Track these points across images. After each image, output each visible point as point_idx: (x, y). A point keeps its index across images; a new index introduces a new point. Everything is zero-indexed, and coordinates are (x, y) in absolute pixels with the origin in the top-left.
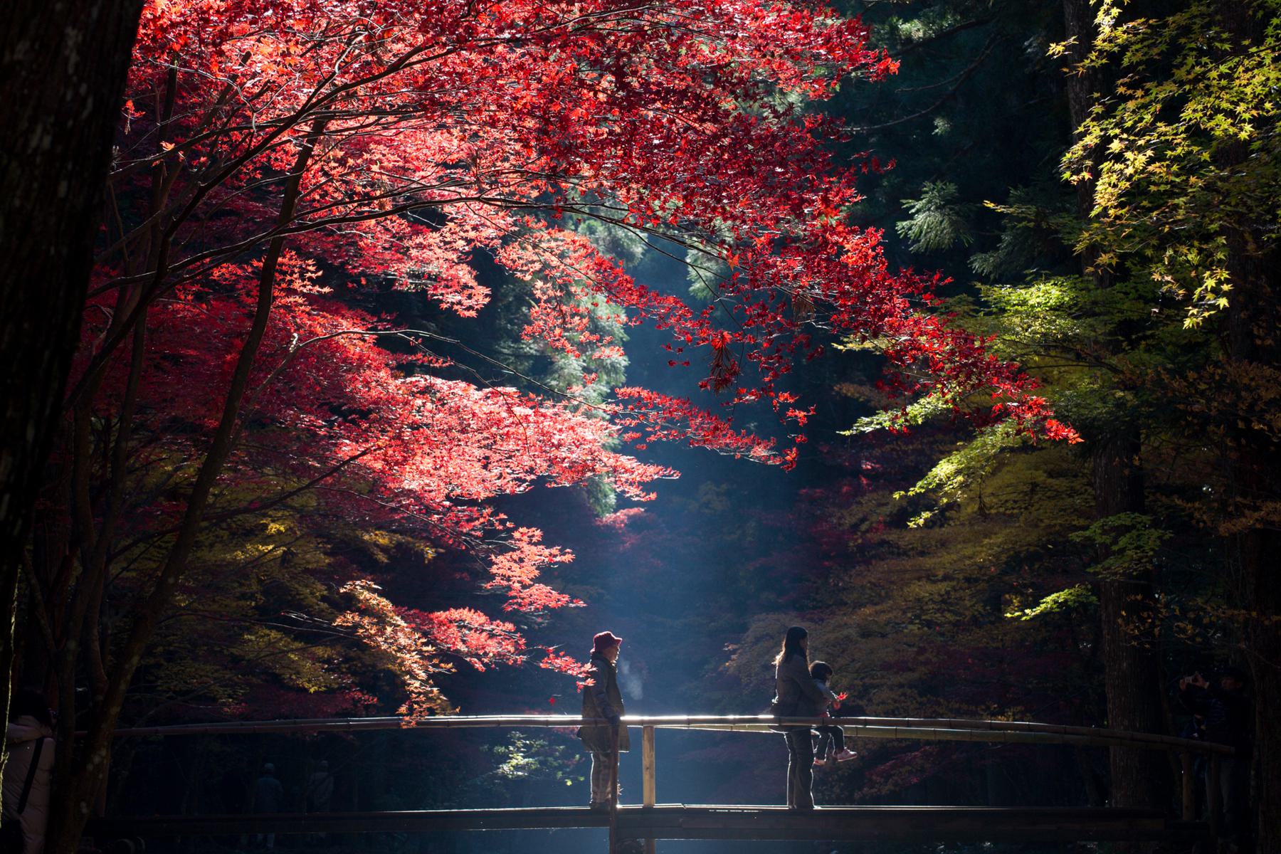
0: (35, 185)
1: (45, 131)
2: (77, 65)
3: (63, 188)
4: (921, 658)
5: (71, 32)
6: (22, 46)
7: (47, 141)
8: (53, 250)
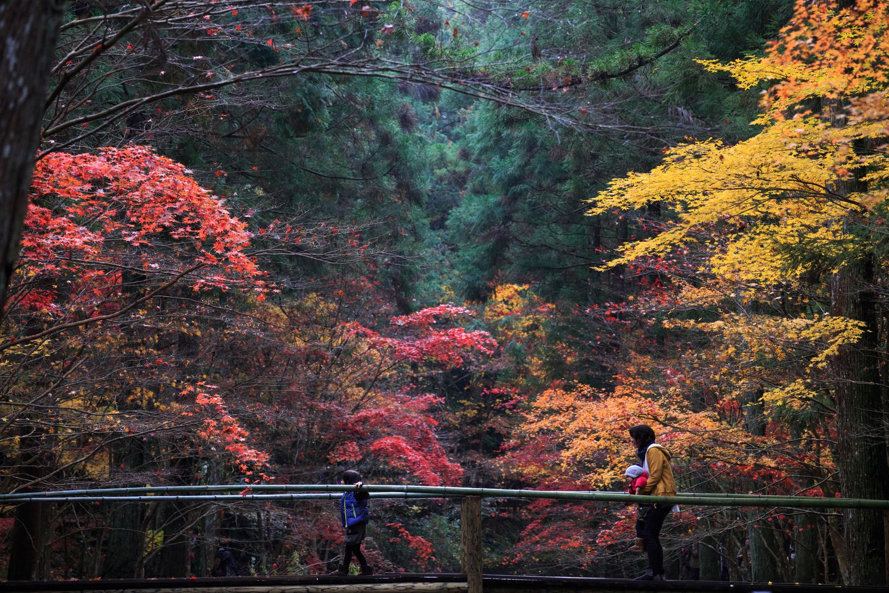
2: (16, 66)
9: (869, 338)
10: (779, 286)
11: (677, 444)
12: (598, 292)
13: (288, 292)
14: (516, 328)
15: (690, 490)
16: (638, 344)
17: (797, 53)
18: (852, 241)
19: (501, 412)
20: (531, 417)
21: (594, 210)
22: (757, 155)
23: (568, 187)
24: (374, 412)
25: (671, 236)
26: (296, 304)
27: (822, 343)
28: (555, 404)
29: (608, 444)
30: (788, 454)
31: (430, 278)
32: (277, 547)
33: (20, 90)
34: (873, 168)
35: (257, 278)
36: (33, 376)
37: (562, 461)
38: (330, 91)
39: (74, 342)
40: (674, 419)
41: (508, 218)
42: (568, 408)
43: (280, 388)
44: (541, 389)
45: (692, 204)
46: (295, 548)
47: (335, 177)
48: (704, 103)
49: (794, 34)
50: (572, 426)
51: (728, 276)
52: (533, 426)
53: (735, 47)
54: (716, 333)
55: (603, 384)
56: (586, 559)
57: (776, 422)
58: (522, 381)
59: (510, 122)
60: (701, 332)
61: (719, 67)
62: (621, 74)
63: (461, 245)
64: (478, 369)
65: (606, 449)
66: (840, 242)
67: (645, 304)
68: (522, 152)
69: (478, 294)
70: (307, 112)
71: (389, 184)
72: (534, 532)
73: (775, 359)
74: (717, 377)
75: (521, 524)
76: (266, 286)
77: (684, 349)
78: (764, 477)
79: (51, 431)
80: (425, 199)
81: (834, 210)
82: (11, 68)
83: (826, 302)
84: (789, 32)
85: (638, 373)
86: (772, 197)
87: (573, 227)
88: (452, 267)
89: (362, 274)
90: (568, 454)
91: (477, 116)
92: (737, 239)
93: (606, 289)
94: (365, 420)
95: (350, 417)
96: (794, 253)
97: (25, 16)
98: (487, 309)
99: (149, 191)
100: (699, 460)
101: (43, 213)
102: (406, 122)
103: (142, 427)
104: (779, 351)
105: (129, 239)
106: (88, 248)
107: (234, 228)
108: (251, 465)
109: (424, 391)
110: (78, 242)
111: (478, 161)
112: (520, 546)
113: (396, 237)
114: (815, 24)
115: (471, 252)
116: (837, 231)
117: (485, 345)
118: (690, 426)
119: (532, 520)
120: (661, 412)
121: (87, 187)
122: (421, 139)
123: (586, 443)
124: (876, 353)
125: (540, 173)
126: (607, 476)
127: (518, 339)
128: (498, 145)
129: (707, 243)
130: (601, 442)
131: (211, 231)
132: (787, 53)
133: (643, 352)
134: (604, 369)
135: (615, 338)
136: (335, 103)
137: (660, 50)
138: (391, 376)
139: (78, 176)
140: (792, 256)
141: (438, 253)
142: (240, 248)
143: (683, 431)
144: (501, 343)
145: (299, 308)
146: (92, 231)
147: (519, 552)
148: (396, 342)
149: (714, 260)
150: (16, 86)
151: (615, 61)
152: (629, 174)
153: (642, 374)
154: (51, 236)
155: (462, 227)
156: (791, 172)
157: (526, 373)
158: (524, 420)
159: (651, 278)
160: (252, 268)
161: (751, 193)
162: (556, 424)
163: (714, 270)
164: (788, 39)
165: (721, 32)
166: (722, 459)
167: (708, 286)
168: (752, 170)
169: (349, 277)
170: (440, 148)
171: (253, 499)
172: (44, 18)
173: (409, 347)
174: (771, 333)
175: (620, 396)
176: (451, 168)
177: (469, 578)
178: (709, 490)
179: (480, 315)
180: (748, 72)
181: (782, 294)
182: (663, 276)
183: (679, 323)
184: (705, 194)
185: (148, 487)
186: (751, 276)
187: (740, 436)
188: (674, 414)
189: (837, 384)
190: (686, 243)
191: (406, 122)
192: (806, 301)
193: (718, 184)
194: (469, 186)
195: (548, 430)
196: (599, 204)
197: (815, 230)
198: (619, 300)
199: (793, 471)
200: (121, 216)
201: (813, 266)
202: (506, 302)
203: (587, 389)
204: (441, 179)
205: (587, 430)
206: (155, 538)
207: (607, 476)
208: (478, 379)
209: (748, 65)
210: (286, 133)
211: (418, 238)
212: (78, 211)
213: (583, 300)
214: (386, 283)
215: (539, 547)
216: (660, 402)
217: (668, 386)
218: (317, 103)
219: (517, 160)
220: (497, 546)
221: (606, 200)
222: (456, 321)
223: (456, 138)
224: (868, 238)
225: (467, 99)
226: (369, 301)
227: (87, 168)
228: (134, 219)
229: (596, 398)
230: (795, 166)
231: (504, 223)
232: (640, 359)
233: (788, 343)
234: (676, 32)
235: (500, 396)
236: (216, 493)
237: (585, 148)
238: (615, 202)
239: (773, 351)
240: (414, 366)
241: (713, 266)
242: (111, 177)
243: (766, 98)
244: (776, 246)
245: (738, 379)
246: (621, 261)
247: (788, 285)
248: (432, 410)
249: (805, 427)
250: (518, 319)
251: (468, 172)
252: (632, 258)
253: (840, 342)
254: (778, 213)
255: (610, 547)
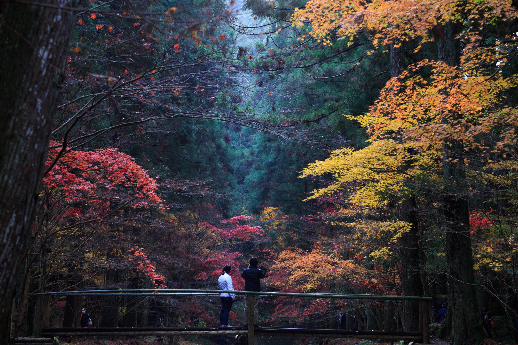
0: (28, 145)
1: (31, 130)
2: (41, 110)
3: (36, 146)
4: (463, 7)
5: (39, 100)
6: (25, 105)
7: (32, 133)
8: (33, 165)
9: (414, 230)
10: (378, 208)
11: (337, 273)
12: (306, 211)
13: (179, 210)
14: (273, 225)
15: (343, 292)
16: (322, 232)
17: (382, 111)
18: (407, 190)
19: (266, 260)
20: (277, 262)
21: (302, 176)
22: (369, 154)
23: (294, 167)
24: (213, 259)
25: (334, 187)
26: (181, 214)
27: (395, 232)
28: (287, 257)
29: (309, 273)
30: (382, 277)
31: (237, 204)
32: (173, 315)
33: (42, 120)
34: (416, 161)
35: (161, 203)
36: (73, 243)
37: (290, 280)
38: (195, 128)
39: (88, 230)
40: (336, 263)
41: (269, 180)
42: (292, 258)
43: (174, 249)
44: (282, 250)
45: (342, 174)
46: (180, 315)
47: (198, 162)
48: (349, 133)
49: (380, 103)
50: (294, 266)
51: (357, 204)
52: (278, 266)
53: (361, 110)
54: (353, 228)
55: (307, 248)
56: (300, 320)
57: (378, 264)
58: (275, 247)
59: (270, 140)
60: (347, 227)
61: (353, 118)
62: (314, 121)
63: (250, 190)
64: (257, 242)
65: (308, 275)
66: (402, 191)
67: (325, 216)
68: (275, 153)
69: (257, 211)
70: (186, 135)
71: (220, 165)
72: (280, 309)
73: (376, 238)
74: (353, 246)
75: (274, 306)
76: (165, 207)
77: (341, 233)
78: (372, 287)
79: (79, 266)
80: (235, 171)
81: (400, 177)
82: (39, 111)
83: (397, 215)
84: (378, 102)
85: (322, 244)
86: (375, 171)
87: (296, 184)
88: (246, 199)
89: (209, 202)
90: (292, 277)
91: (257, 138)
92: (361, 188)
93: (309, 209)
94: (210, 262)
95: (202, 261)
96: (383, 195)
97: (45, 89)
98: (261, 217)
99: (116, 167)
100: (346, 280)
101: (73, 176)
102: (227, 140)
103: (116, 265)
104: (378, 235)
105: (107, 187)
106: (90, 191)
107: (151, 182)
108: (157, 281)
109: (234, 251)
110: (86, 188)
111: (257, 156)
112: (273, 315)
113: (222, 187)
114: (389, 100)
115: (254, 194)
116: (401, 186)
117: (259, 232)
118: (343, 266)
119: (279, 304)
120: (331, 260)
121: (91, 165)
122: (234, 147)
123: (300, 273)
124: (417, 236)
125: (282, 161)
126: (308, 286)
127: (274, 230)
128: (265, 150)
129: (349, 190)
130: (306, 272)
131: (141, 184)
132: (377, 111)
133: (324, 235)
134: (308, 242)
135: (312, 229)
136: (197, 133)
137: (331, 111)
138: (221, 244)
139: (87, 161)
140: (383, 196)
141: (241, 194)
142: (153, 191)
143: (340, 268)
144: (266, 231)
145: (182, 216)
146: (92, 183)
147: (274, 317)
148: (222, 230)
149: (351, 197)
150: (41, 118)
151: (312, 115)
152: (316, 161)
153: (323, 244)
154: (75, 185)
155: (250, 183)
156: (382, 161)
157: (277, 244)
158: (275, 263)
159: (325, 204)
160: (158, 199)
161: (366, 170)
162: (287, 265)
163: (351, 202)
164: (378, 105)
165: (355, 104)
166: (356, 279)
167: (350, 208)
168: (367, 160)
169: (204, 203)
170: (242, 151)
171: (159, 295)
172: (53, 90)
173: (228, 233)
174: (375, 228)
175: (313, 254)
176: (246, 159)
177: (249, 329)
178: (350, 292)
179: (258, 219)
180: (365, 120)
181: (380, 212)
182: (332, 204)
183: (338, 223)
184: (347, 170)
185: (121, 290)
186: (366, 204)
187: (364, 271)
188: (337, 261)
189: (401, 249)
190: (339, 190)
191: (227, 140)
192: (389, 215)
193: (353, 166)
194: (253, 166)
195: (284, 267)
196: (304, 173)
197: (392, 185)
198: (314, 214)
199: (384, 284)
200: (104, 178)
201: (391, 200)
202: (269, 214)
203: (300, 250)
204: (242, 163)
205: (304, 267)
206: (123, 310)
207: (308, 286)
208: (257, 246)
209: (365, 117)
210: (177, 144)
211: (233, 188)
212: (87, 175)
213: (300, 213)
214: (219, 206)
215: (281, 316)
216: (331, 256)
217: (333, 249)
218: (190, 132)
219: (273, 156)
220: (264, 315)
221: (306, 172)
222: (248, 222)
223: (248, 147)
224: (413, 189)
225: (253, 131)
226: (211, 213)
227: (91, 157)
228: (110, 178)
229: (305, 254)
230: (384, 159)
231: (267, 182)
232: (323, 238)
233: (382, 232)
234: (337, 104)
235: (266, 253)
236: (144, 292)
237: (301, 151)
238: (310, 172)
239: (376, 235)
240: (231, 241)
241: (350, 200)
242: (101, 161)
243: (369, 129)
244: (377, 192)
245: (362, 247)
246: (313, 197)
247: (382, 208)
248: (238, 258)
249: (389, 266)
250: (273, 221)
251: (253, 161)
252: (317, 196)
253: (402, 232)
254: (378, 178)
255: (309, 315)
